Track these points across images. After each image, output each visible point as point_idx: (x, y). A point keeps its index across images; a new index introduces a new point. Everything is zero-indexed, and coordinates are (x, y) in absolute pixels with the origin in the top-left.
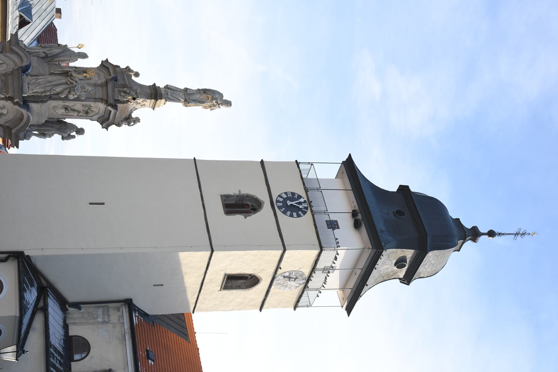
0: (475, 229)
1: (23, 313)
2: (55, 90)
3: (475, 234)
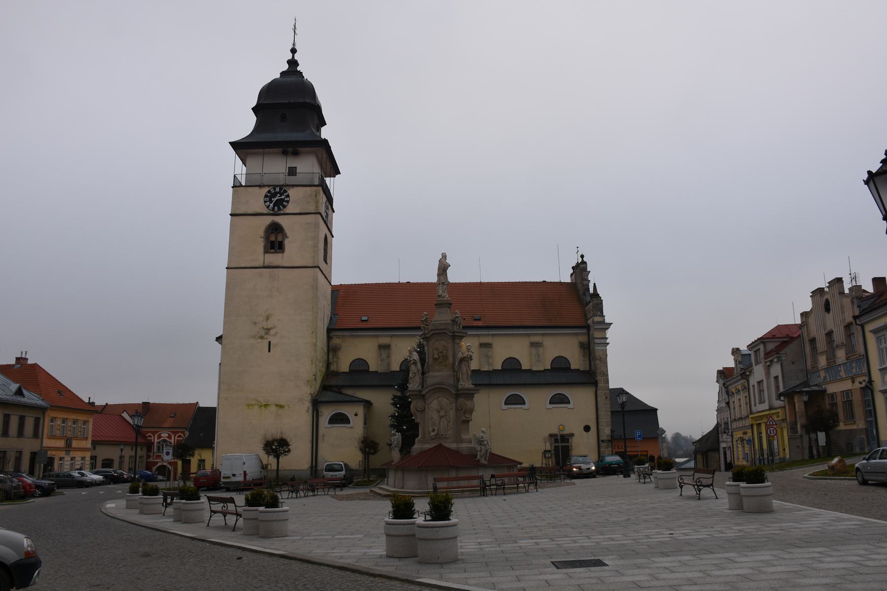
0: (289, 62)
1: (357, 399)
3: (293, 63)
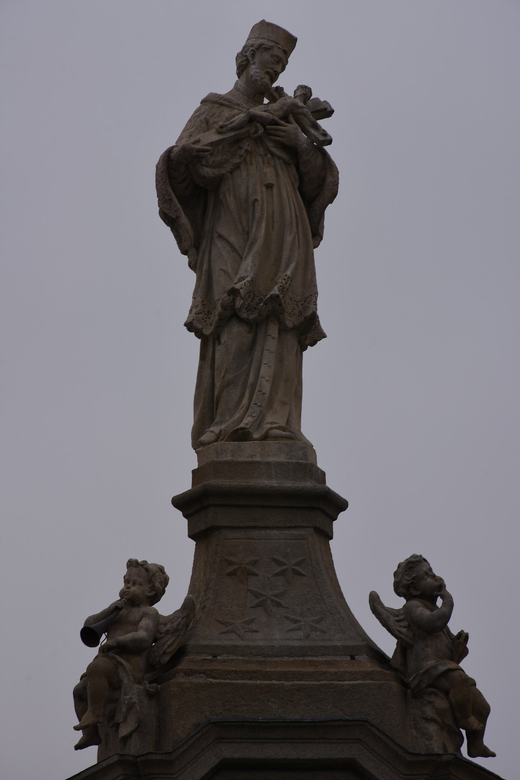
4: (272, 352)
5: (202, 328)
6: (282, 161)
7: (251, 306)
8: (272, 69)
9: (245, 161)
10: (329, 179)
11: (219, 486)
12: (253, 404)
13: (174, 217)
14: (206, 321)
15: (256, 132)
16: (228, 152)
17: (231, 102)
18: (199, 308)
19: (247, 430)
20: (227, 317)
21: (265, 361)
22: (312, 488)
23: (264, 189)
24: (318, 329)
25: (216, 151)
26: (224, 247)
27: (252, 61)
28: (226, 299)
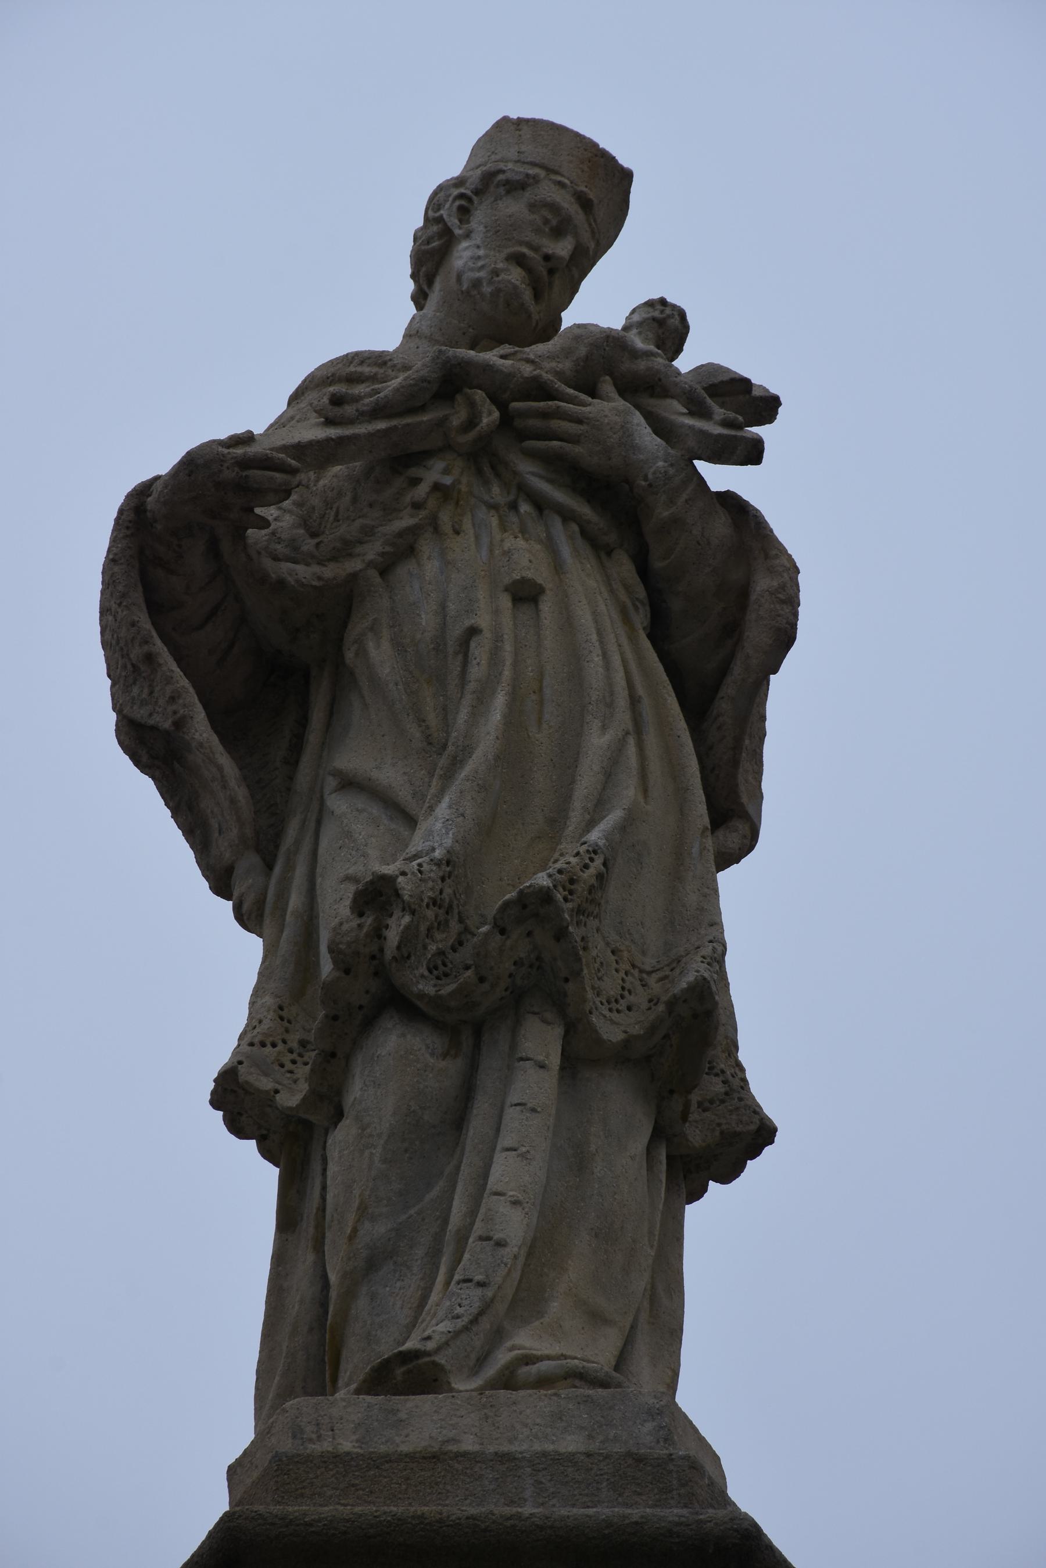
2: (428, 803)
4: (533, 1110)
5: (277, 1092)
6: (575, 528)
7: (451, 963)
8: (536, 249)
9: (436, 529)
10: (762, 584)
11: (292, 1517)
12: (458, 1283)
13: (167, 725)
14: (291, 1072)
15: (471, 423)
16: (371, 505)
17: (385, 363)
18: (266, 1027)
19: (427, 1359)
20: (361, 1007)
21: (507, 1140)
22: (683, 1519)
23: (505, 602)
24: (740, 1099)
25: (332, 518)
26: (358, 810)
27: (460, 228)
28: (346, 927)
